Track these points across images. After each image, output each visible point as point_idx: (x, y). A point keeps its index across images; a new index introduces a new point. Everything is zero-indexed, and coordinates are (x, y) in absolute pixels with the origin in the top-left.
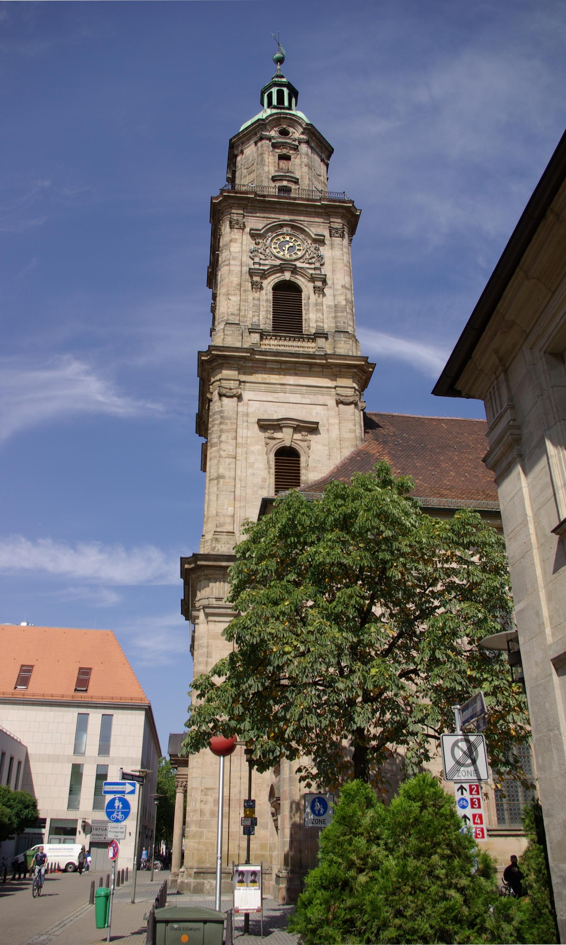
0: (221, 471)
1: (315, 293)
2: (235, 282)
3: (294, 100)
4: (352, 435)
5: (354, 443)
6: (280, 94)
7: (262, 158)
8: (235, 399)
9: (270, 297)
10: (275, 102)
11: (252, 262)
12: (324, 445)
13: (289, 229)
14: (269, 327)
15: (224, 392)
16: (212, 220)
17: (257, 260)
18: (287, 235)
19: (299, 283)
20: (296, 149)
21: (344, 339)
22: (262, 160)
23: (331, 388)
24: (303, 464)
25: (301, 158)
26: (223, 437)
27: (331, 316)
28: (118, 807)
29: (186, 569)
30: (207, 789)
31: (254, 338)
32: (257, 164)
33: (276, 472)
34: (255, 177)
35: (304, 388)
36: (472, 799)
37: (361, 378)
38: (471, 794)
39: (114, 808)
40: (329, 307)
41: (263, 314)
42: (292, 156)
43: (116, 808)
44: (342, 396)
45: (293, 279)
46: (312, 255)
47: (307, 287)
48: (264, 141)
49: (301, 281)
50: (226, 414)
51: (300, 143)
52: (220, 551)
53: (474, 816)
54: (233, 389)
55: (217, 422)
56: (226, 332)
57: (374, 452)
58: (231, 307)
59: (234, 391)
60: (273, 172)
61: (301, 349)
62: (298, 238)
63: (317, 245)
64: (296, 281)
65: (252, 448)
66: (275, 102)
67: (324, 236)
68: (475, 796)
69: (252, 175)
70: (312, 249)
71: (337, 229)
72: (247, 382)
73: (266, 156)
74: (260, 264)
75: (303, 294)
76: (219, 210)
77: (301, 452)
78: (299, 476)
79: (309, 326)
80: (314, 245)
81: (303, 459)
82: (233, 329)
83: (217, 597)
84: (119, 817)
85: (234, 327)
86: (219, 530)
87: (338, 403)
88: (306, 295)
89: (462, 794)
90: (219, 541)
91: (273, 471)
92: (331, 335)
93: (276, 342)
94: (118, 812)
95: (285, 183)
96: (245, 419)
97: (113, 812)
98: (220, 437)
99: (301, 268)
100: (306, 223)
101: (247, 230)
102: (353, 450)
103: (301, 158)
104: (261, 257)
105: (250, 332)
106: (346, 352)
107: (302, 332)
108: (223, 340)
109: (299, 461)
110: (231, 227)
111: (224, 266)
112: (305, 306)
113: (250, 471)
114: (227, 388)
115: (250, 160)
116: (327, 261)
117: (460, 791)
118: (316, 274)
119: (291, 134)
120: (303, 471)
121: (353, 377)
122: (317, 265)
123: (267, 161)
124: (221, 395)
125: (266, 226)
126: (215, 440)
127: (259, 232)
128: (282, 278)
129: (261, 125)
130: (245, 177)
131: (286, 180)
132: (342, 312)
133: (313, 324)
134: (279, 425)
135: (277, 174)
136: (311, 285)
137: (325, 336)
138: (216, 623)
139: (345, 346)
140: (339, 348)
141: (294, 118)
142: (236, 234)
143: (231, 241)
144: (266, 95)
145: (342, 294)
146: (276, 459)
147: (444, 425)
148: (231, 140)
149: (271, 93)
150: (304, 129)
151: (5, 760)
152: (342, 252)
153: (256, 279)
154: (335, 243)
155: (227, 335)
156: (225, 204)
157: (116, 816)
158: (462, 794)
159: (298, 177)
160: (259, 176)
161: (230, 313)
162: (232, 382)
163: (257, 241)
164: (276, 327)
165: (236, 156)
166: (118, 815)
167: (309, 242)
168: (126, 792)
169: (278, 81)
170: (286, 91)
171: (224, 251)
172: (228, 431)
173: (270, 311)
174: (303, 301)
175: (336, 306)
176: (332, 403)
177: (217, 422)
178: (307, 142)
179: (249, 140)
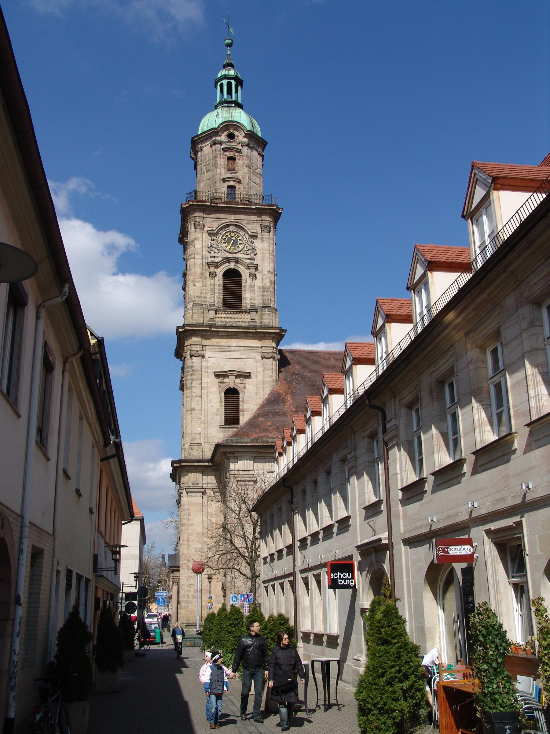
3: (239, 88)
11: (210, 255)
17: (212, 254)
18: (233, 232)
19: (240, 271)
20: (240, 151)
24: (241, 399)
26: (194, 384)
33: (225, 404)
40: (259, 287)
41: (216, 295)
42: (237, 158)
45: (236, 268)
47: (245, 273)
48: (217, 146)
49: (241, 269)
59: (200, 353)
63: (252, 239)
64: (238, 269)
71: (266, 226)
74: (214, 257)
80: (250, 240)
81: (241, 395)
82: (198, 308)
86: (192, 442)
87: (262, 358)
95: (232, 183)
98: (192, 383)
109: (239, 397)
119: (236, 137)
120: (241, 404)
122: (252, 255)
124: (191, 356)
126: (189, 385)
127: (213, 232)
131: (232, 181)
132: (267, 291)
133: (248, 302)
134: (227, 374)
136: (248, 271)
140: (264, 319)
143: (195, 239)
146: (225, 396)
148: (193, 138)
155: (194, 313)
162: (198, 346)
170: (234, 83)
172: (196, 380)
178: (248, 145)
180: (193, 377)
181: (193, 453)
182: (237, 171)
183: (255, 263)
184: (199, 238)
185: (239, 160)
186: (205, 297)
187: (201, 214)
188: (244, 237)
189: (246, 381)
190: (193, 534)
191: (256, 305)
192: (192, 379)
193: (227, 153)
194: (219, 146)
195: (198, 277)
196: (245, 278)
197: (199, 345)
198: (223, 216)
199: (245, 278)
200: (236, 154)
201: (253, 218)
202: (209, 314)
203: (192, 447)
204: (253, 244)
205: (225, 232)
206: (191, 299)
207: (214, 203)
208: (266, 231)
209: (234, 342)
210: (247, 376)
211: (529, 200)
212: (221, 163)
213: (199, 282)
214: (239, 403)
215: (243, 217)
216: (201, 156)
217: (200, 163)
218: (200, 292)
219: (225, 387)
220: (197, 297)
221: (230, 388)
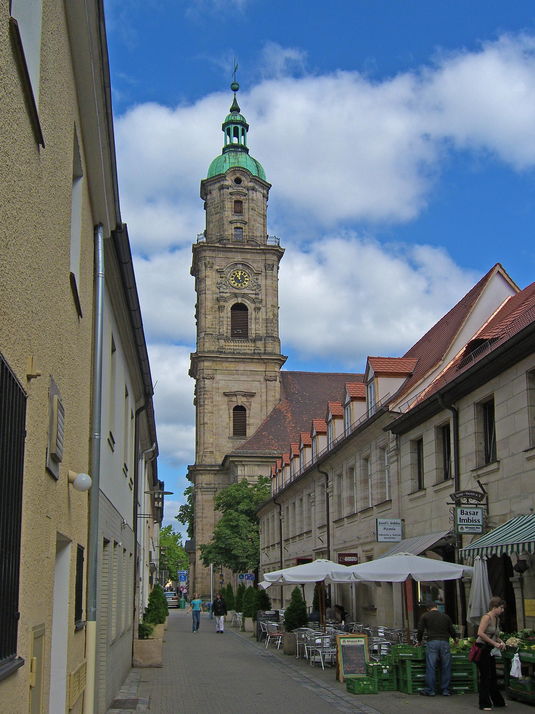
2: (209, 306)
7: (224, 204)
9: (229, 315)
12: (259, 404)
14: (229, 334)
17: (222, 290)
19: (247, 305)
26: (206, 402)
27: (264, 325)
42: (243, 201)
45: (243, 302)
49: (248, 303)
56: (205, 340)
58: (208, 323)
59: (211, 376)
64: (244, 303)
65: (221, 407)
71: (269, 264)
73: (226, 203)
74: (223, 292)
75: (249, 311)
77: (247, 409)
80: (255, 277)
81: (247, 412)
82: (209, 338)
86: (205, 450)
93: (232, 344)
95: (239, 225)
96: (217, 391)
98: (204, 402)
113: (220, 419)
116: (263, 288)
120: (247, 419)
128: (236, 302)
132: (271, 323)
140: (268, 347)
151: (54, 664)
153: (222, 303)
156: (201, 249)
170: (240, 128)
172: (208, 399)
174: (249, 317)
175: (267, 319)
176: (262, 380)
188: (250, 274)
190: (207, 525)
192: (205, 398)
193: (234, 197)
194: (227, 190)
210: (252, 395)
212: (229, 206)
215: (249, 256)
218: (211, 323)
220: (209, 328)
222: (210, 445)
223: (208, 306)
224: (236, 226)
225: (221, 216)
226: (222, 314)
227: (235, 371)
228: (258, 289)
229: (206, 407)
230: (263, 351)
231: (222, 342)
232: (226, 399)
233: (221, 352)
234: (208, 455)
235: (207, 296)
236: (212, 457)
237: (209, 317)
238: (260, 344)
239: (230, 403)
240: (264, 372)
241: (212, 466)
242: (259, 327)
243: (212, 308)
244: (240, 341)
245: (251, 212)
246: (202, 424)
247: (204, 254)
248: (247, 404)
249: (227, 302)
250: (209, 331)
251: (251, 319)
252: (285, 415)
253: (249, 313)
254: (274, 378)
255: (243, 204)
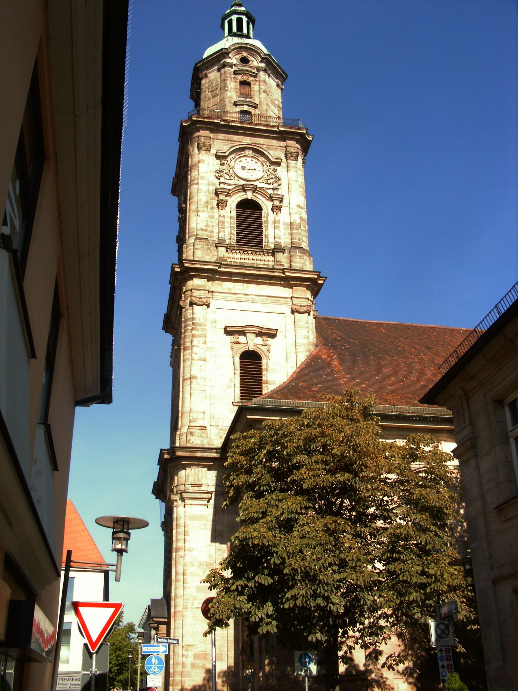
0: (194, 373)
1: (273, 212)
3: (251, 26)
4: (306, 341)
5: (308, 348)
6: (240, 21)
7: (226, 84)
8: (205, 307)
9: (234, 214)
10: (235, 29)
11: (218, 181)
13: (251, 152)
14: (234, 242)
15: (195, 301)
16: (180, 140)
17: (222, 180)
18: (249, 157)
19: (260, 202)
20: (255, 76)
21: (299, 254)
22: (225, 86)
23: (288, 298)
24: (264, 367)
25: (259, 85)
26: (195, 342)
28: (155, 663)
29: (166, 459)
30: (188, 645)
31: (221, 252)
32: (220, 89)
33: (241, 373)
34: (219, 101)
35: (265, 298)
36: (446, 656)
37: (313, 289)
38: (446, 653)
39: (152, 664)
40: (285, 224)
41: (227, 230)
42: (252, 83)
43: (153, 664)
44: (297, 306)
45: (254, 198)
46: (271, 176)
47: (266, 205)
48: (227, 68)
49: (262, 201)
50: (197, 321)
51: (258, 70)
52: (194, 443)
53: (448, 665)
54: (203, 298)
55: (190, 328)
56: (196, 246)
57: (325, 357)
59: (204, 300)
60: (235, 97)
61: (262, 263)
62: (259, 160)
63: (275, 167)
64: (257, 200)
66: (235, 29)
67: (282, 159)
68: (448, 655)
69: (216, 98)
70: (271, 171)
71: (292, 153)
72: (215, 292)
74: (225, 183)
75: (263, 212)
76: (188, 132)
77: (263, 356)
78: (261, 377)
79: (268, 242)
80: (272, 167)
81: (264, 362)
82: (202, 243)
83: (193, 483)
84: (155, 671)
85: (203, 242)
86: (192, 424)
87: (293, 312)
88: (265, 213)
89: (441, 653)
90: (193, 435)
91: (238, 372)
92: (287, 250)
93: (239, 256)
94: (155, 667)
95: (246, 108)
97: (151, 667)
98: (192, 341)
99: (261, 188)
100: (265, 146)
101: (213, 151)
102: (307, 354)
103: (259, 85)
104: (226, 178)
105: (216, 247)
106: (301, 266)
107: (262, 247)
108: (194, 253)
109: (261, 363)
110: (199, 149)
111: (193, 184)
112: (265, 223)
114: (197, 297)
115: (214, 85)
116: (284, 181)
117: (440, 652)
118: (274, 194)
119: (250, 63)
120: (264, 373)
121: (308, 288)
122: (276, 185)
123: (229, 86)
124: (191, 304)
125: (230, 148)
126: (188, 344)
127: (224, 154)
128: (244, 197)
129: (223, 53)
130: (209, 99)
131: (247, 105)
132: (297, 229)
133: (271, 240)
134: (243, 331)
135: (238, 99)
136: (270, 204)
137: (282, 250)
138: (192, 506)
139: (300, 260)
140: (295, 262)
141: (254, 48)
142: (203, 156)
143: (199, 162)
144: (226, 21)
145: (297, 213)
146: (241, 362)
147: (383, 330)
148: (196, 64)
149: (231, 20)
150: (262, 58)
152: (296, 174)
153: (222, 197)
154: (291, 165)
155: (197, 249)
157: (153, 670)
158: (441, 653)
159: (257, 103)
160: (222, 100)
161: (199, 229)
162: (202, 292)
163: (223, 162)
164: (238, 243)
165: (201, 79)
166: (155, 669)
167: (268, 164)
168: (160, 652)
169: (238, 10)
170: (245, 19)
171: (193, 170)
172: (199, 336)
173: (234, 228)
174: (263, 219)
177: (190, 328)
178: (265, 70)
179: (213, 66)
180: (194, 332)
181: (194, 440)
182: (252, 96)
183: (279, 192)
184: (204, 160)
185: (255, 85)
186: (212, 232)
187: (206, 133)
188: (264, 163)
189: (270, 341)
190: (192, 564)
191: (283, 246)
192: (193, 336)
193: (239, 77)
194: (230, 69)
195: (202, 206)
196: (266, 211)
197: (204, 290)
198: (235, 137)
199: (266, 211)
200: (251, 79)
201: (274, 142)
202: (218, 252)
203: (192, 431)
204: (276, 173)
205: (239, 156)
206: (193, 232)
207: (224, 121)
208: (293, 158)
209: (253, 289)
210: (272, 334)
211: (481, 324)
212: (232, 86)
213: (204, 211)
214: (261, 372)
215: (262, 141)
216: (206, 83)
217: (204, 90)
218: (205, 224)
219: (242, 349)
220: (202, 230)
221: (249, 350)
222: (201, 416)
223: (200, 200)
224: (242, 109)
225: (222, 97)
226: (222, 212)
227: (243, 296)
228: (276, 182)
229: (195, 349)
230: (286, 266)
231: (222, 251)
232: (229, 339)
233: (221, 265)
234: (197, 432)
235: (200, 187)
236: (204, 435)
237: (204, 216)
238: (282, 258)
239: (235, 345)
240: (290, 300)
241: (204, 449)
242: (280, 234)
243: (207, 202)
244: (250, 253)
245: (263, 95)
246: (187, 379)
247: (190, 284)
248: (264, 348)
249: (230, 196)
250: (201, 234)
251: (267, 222)
252: (329, 363)
253: (263, 214)
254: (306, 309)
255: (252, 86)
